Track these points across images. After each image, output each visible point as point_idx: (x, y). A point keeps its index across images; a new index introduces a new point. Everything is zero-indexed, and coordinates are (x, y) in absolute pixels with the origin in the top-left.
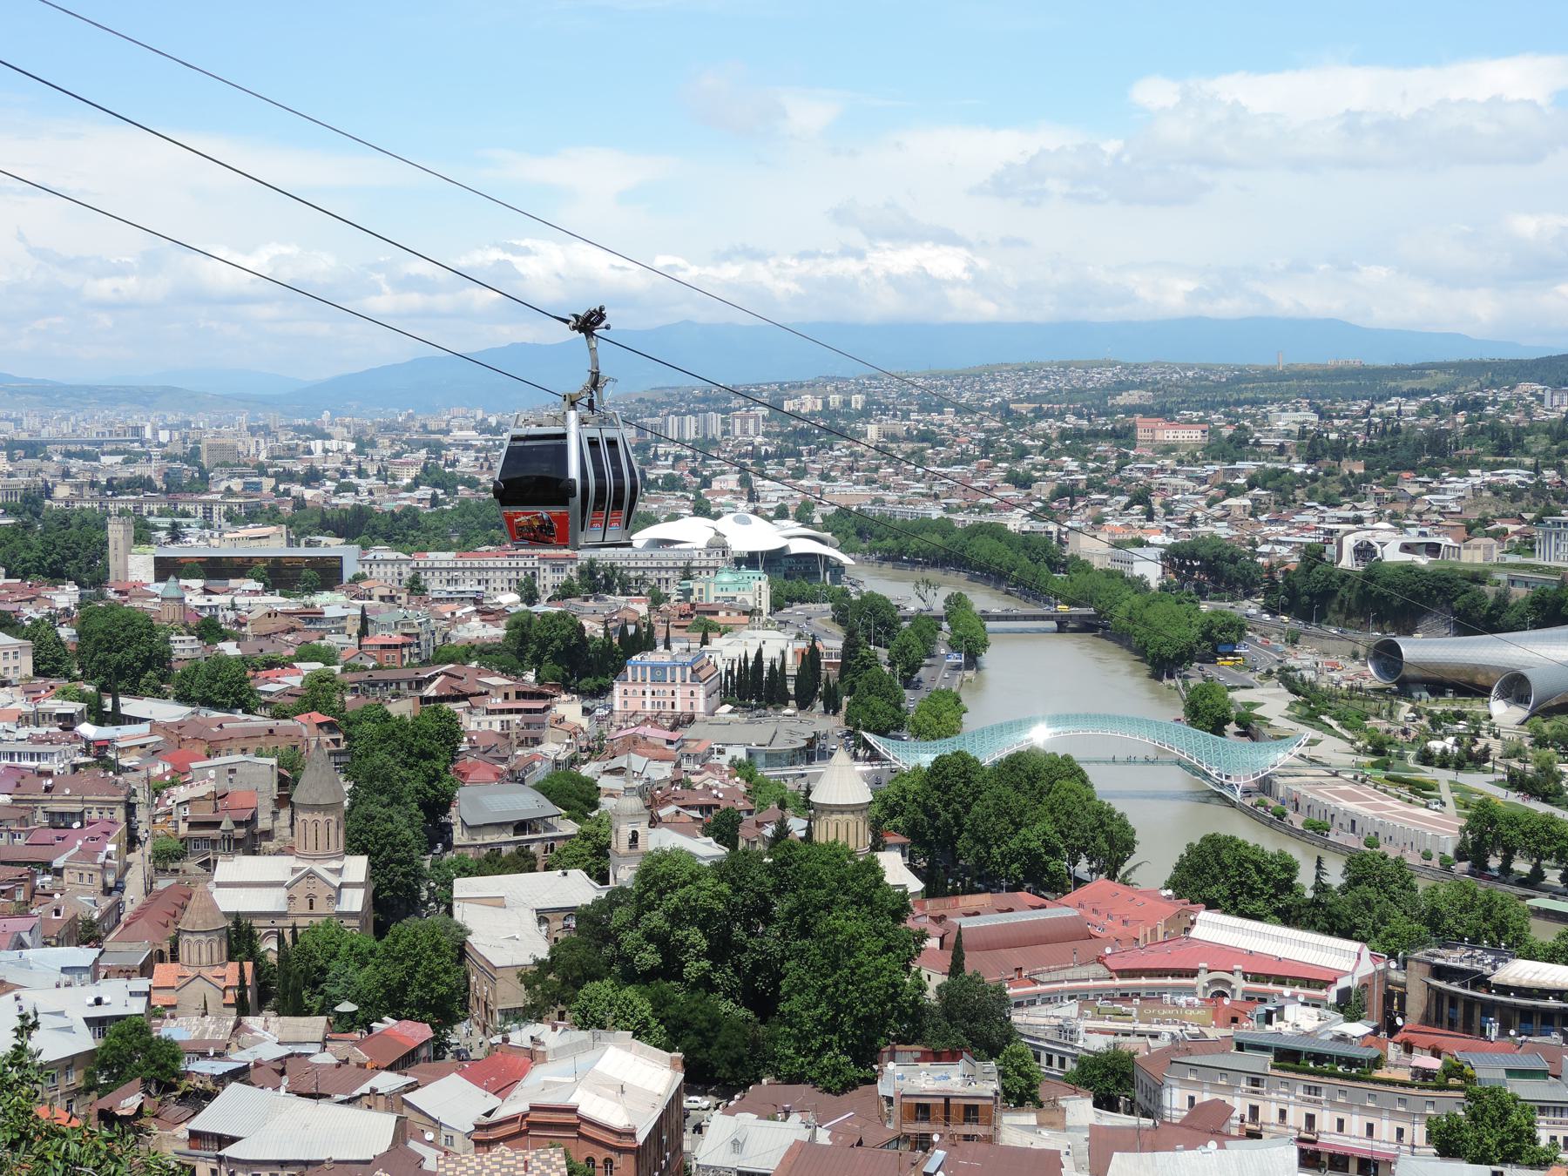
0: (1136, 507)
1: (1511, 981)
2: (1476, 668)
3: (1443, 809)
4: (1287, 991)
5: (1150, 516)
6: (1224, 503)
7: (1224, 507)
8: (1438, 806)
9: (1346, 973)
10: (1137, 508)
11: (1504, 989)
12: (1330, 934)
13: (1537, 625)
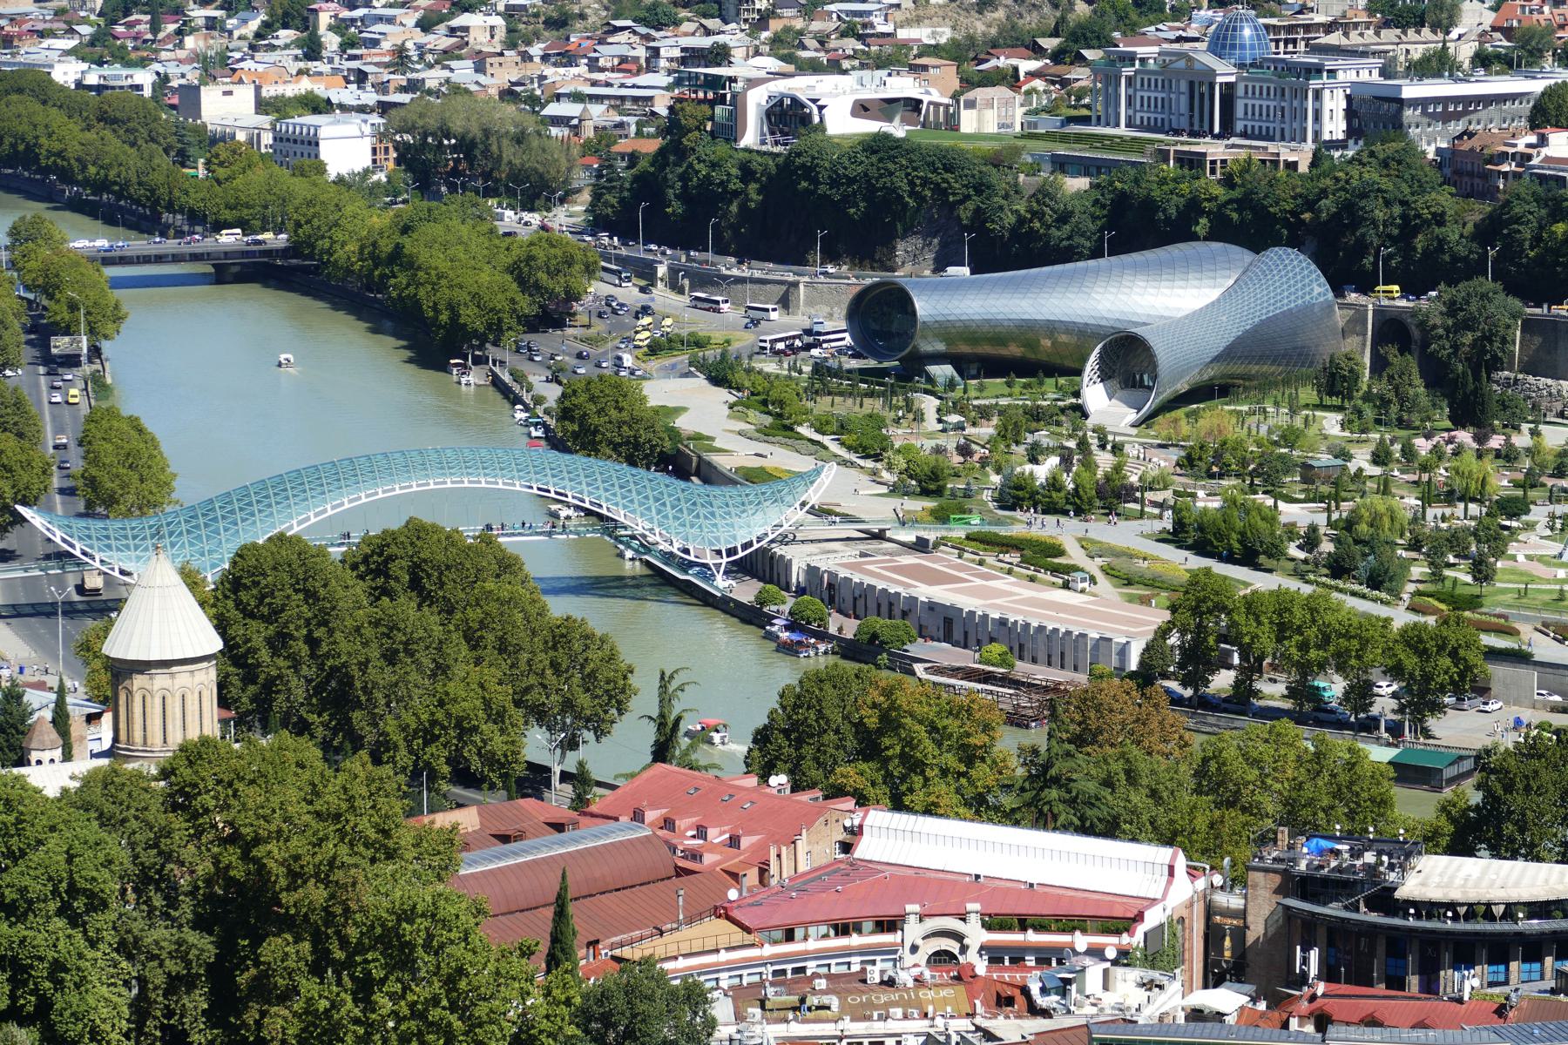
0: (282, 33)
1: (1435, 894)
2: (1051, 327)
3: (1094, 588)
4: (1081, 941)
5: (312, 50)
6: (455, 23)
7: (452, 31)
8: (1086, 585)
9: (1154, 901)
10: (286, 35)
11: (1430, 909)
12: (1043, 819)
13: (1120, 247)
